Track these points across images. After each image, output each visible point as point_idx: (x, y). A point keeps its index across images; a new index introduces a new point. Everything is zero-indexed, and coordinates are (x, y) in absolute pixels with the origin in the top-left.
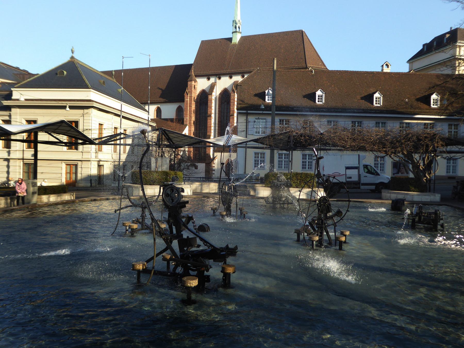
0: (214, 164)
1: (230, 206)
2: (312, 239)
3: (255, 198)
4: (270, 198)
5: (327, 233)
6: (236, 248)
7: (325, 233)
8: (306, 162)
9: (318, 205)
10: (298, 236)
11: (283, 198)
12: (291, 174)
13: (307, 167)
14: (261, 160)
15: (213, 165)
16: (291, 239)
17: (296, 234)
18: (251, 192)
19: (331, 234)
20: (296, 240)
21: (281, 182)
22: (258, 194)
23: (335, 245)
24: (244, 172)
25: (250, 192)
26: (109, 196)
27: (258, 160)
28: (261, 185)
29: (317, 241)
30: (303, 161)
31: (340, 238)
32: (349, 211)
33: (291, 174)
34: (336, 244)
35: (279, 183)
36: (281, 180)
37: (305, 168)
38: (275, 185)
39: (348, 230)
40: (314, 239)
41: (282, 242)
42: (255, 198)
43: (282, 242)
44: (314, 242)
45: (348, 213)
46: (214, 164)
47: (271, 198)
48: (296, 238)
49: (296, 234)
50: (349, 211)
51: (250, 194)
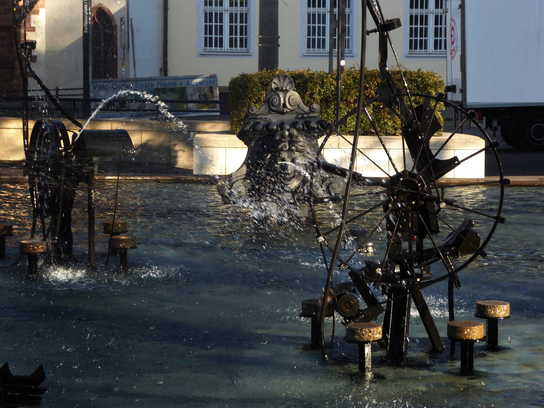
0: (33, 29)
1: (67, 222)
2: (357, 337)
3: (191, 182)
4: (239, 183)
5: (424, 310)
6: (40, 374)
7: (414, 313)
8: (424, 19)
9: (386, 208)
10: (317, 327)
11: (290, 180)
12: (337, 80)
13: (431, 38)
14: (231, 15)
15: (30, 36)
16: (290, 341)
17: (309, 320)
18: (180, 154)
19: (435, 313)
20: (308, 342)
21: (282, 113)
22: (205, 161)
23: (452, 358)
24: (160, 65)
25: (176, 157)
26: (182, 114)
27: (221, 14)
28: (220, 126)
29: (377, 345)
30: (411, 17)
31: (462, 331)
32: (502, 221)
33: (337, 80)
34: (452, 353)
35: (274, 119)
36: (284, 105)
37: (423, 45)
38: (260, 127)
39: (504, 300)
40: (366, 338)
41: (250, 353)
42: (191, 182)
43: (250, 353)
44: (368, 350)
45: (501, 229)
46: (33, 29)
47: (245, 179)
48: (309, 335)
49: (309, 320)
50: (502, 221)
51: (175, 163)
